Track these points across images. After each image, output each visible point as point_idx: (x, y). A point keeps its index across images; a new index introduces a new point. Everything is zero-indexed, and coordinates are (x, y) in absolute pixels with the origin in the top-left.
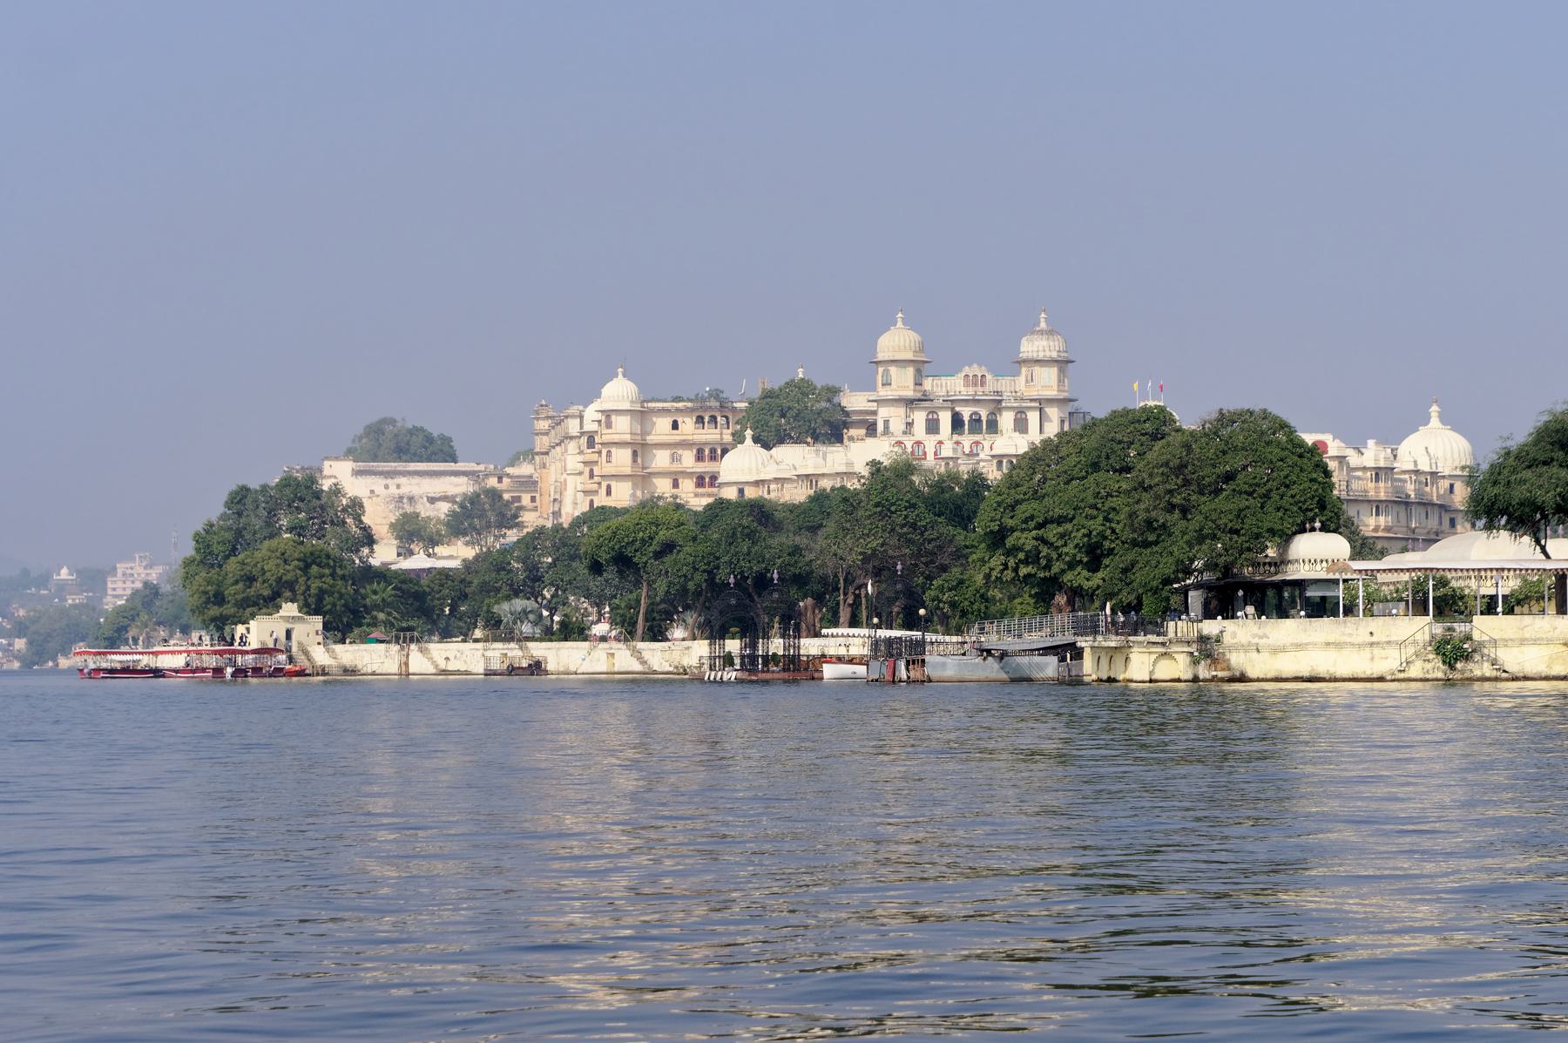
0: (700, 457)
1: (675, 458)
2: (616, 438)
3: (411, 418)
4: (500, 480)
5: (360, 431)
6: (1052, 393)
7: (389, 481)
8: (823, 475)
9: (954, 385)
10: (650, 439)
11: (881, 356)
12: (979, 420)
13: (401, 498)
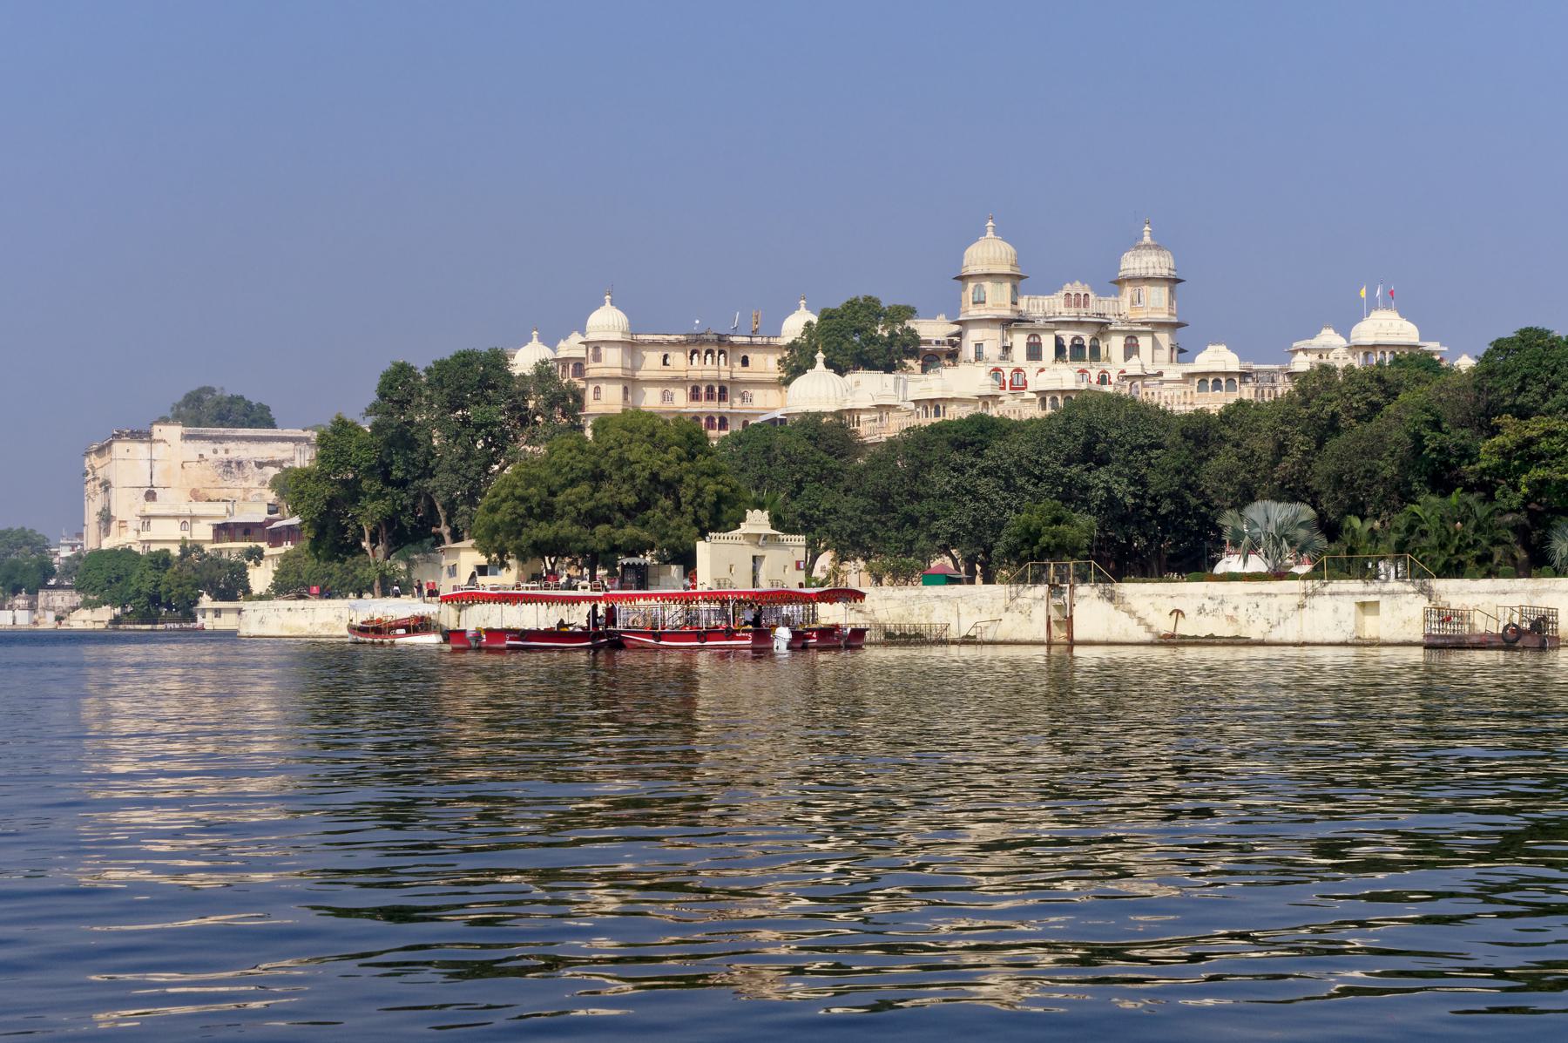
0: (695, 395)
1: (666, 397)
2: (606, 372)
3: (229, 386)
5: (179, 398)
6: (1163, 316)
7: (217, 446)
8: (952, 400)
9: (1051, 305)
10: (640, 374)
11: (971, 270)
12: (1082, 347)
13: (229, 462)
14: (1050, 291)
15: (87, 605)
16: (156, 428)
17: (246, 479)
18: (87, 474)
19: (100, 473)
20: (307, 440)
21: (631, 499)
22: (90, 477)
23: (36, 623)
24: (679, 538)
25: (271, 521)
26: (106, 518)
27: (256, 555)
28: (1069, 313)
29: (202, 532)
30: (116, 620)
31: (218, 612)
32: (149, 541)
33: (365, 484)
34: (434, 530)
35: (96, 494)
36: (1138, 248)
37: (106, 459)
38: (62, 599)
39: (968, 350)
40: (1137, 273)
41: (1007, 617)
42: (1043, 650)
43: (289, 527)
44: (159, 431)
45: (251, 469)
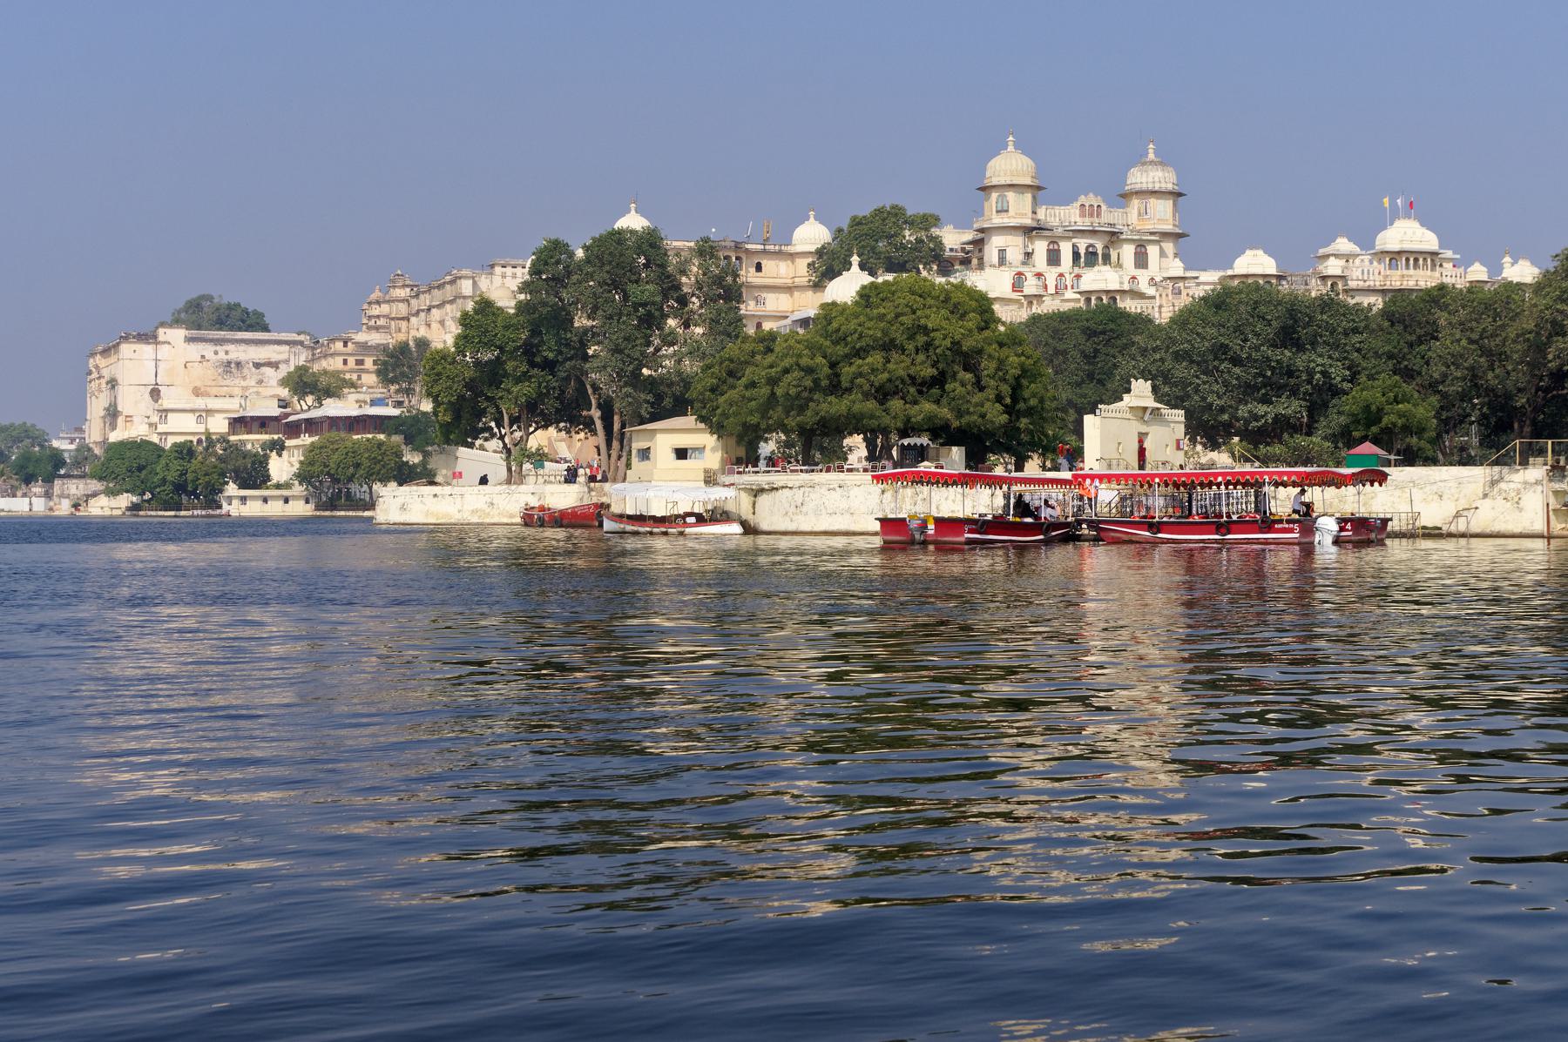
3: (226, 294)
4: (345, 345)
5: (181, 305)
11: (995, 181)
12: (1095, 254)
14: (1066, 201)
15: (111, 493)
16: (161, 331)
17: (244, 378)
18: (90, 373)
19: (105, 372)
20: (301, 343)
21: (929, 372)
22: (95, 375)
23: (51, 509)
24: (983, 416)
25: (287, 415)
26: (112, 414)
27: (279, 447)
28: (1083, 223)
29: (219, 425)
30: (135, 508)
31: (243, 499)
32: (167, 434)
33: (510, 366)
34: (585, 413)
35: (100, 390)
36: (1144, 164)
37: (113, 359)
38: (75, 488)
39: (991, 253)
40: (1144, 187)
41: (1485, 505)
42: (1540, 544)
43: (307, 420)
44: (163, 334)
45: (249, 370)
